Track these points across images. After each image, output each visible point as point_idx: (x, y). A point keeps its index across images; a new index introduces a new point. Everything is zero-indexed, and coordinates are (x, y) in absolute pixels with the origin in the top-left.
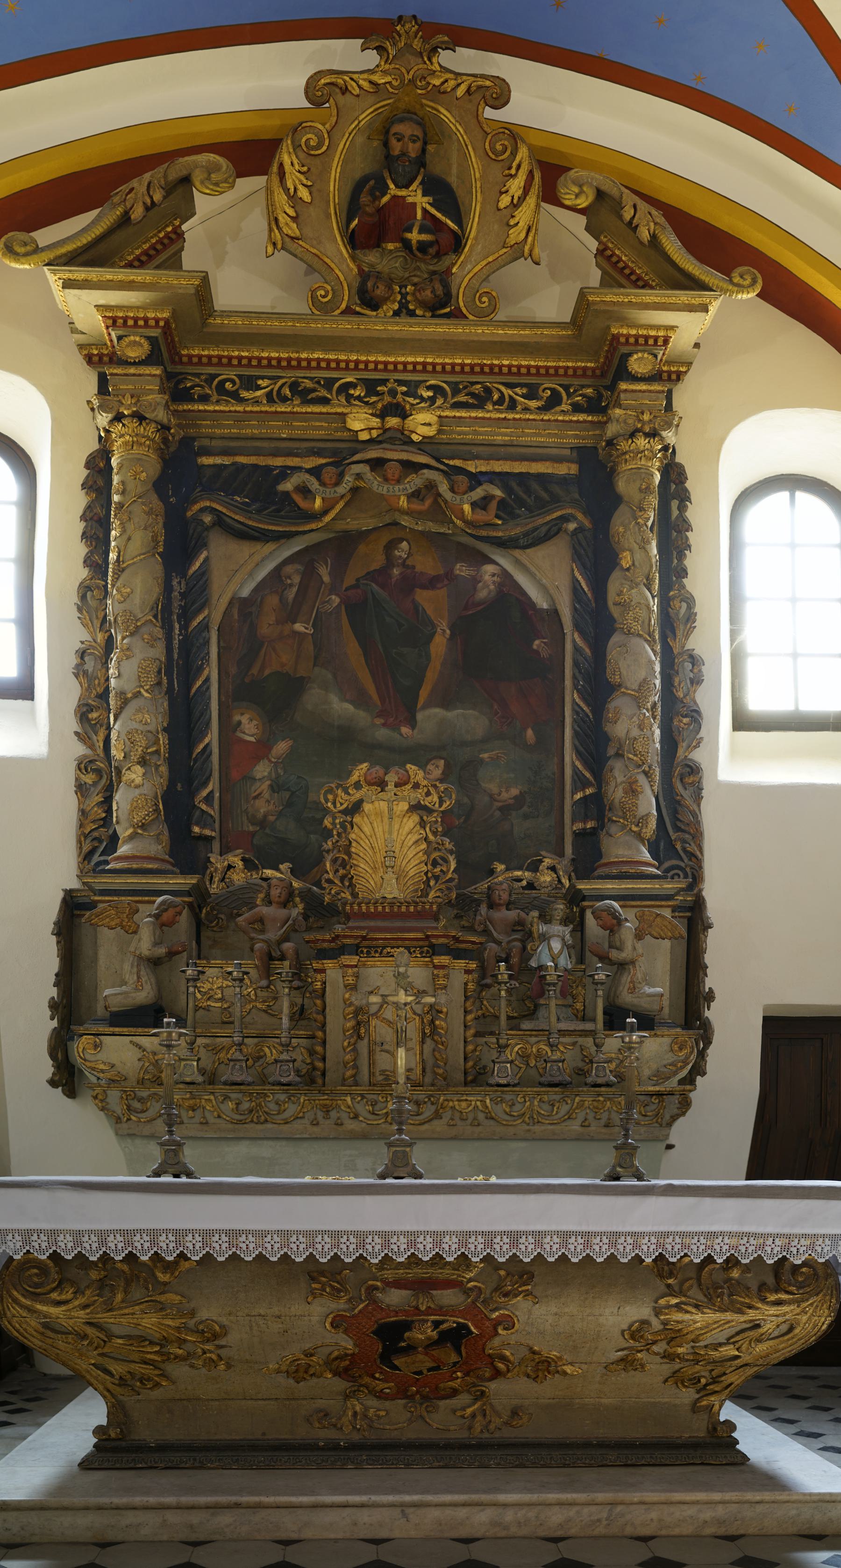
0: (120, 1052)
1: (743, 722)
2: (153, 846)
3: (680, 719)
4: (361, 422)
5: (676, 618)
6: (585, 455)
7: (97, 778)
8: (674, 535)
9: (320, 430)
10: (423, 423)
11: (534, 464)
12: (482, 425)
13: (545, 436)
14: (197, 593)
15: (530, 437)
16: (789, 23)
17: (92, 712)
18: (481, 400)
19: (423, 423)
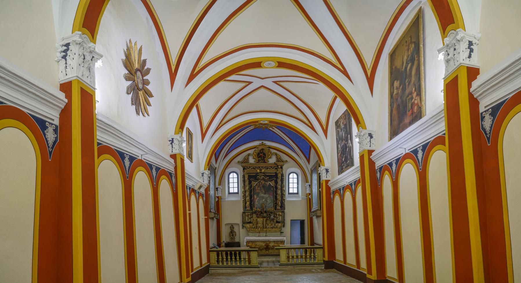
0: (248, 226)
1: (289, 193)
2: (249, 208)
3: (283, 195)
4: (258, 171)
5: (282, 187)
6: (276, 173)
7: (245, 202)
8: (282, 180)
9: (255, 172)
10: (263, 171)
11: (180, 223)
12: (268, 171)
13: (272, 171)
14: (251, 186)
15: (271, 172)
16: (516, 58)
17: (244, 196)
18: (268, 168)
19: (263, 171)
